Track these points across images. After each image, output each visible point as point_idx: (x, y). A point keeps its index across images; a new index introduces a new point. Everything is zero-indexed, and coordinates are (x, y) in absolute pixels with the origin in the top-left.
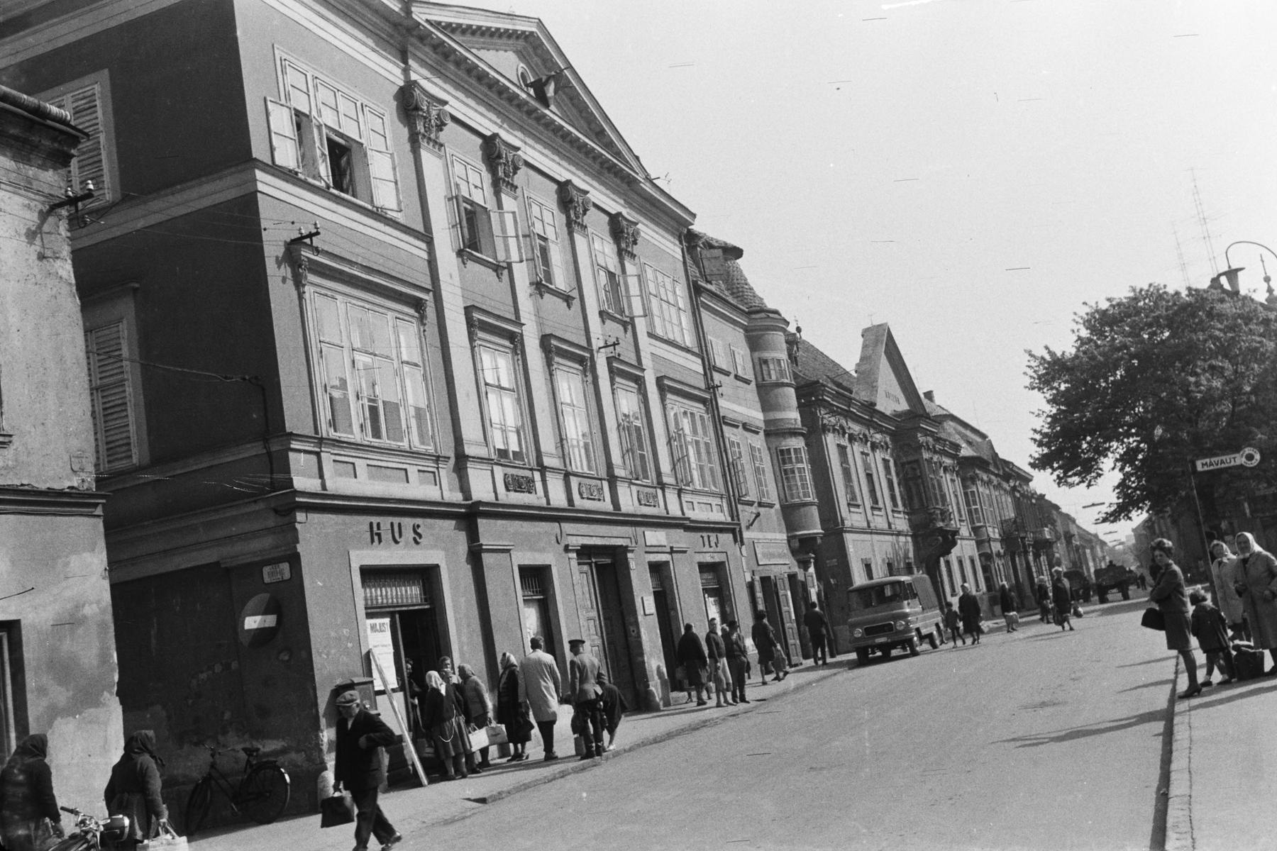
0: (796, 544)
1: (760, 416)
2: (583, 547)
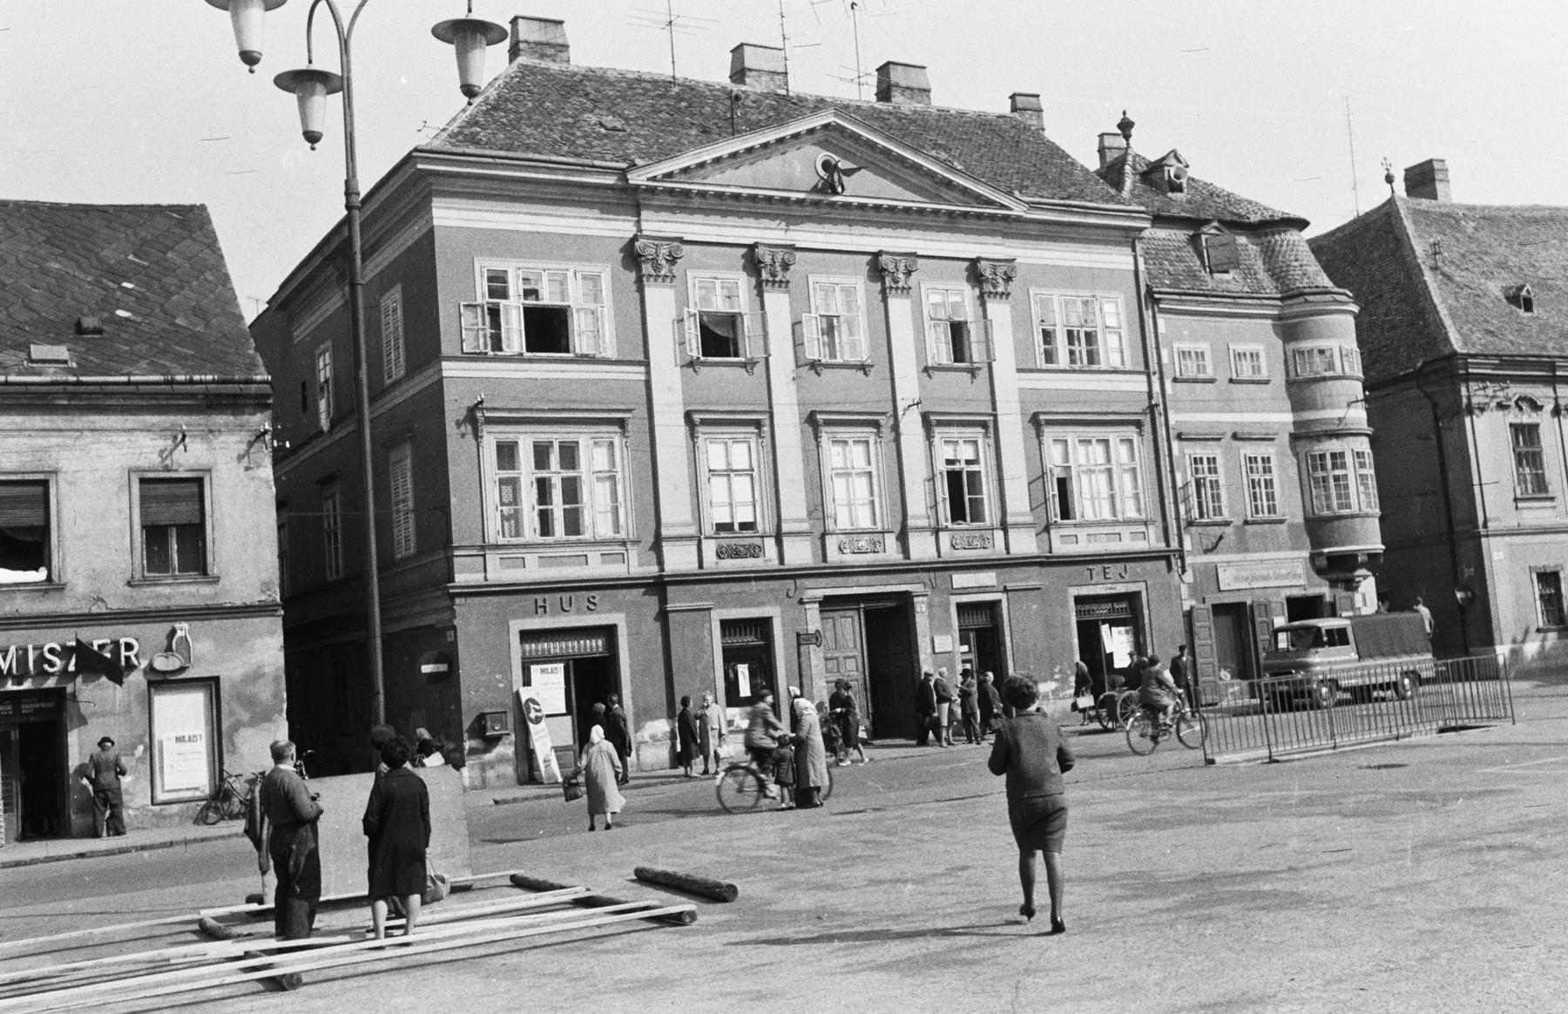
0: (1323, 563)
1: (1288, 417)
2: (826, 597)
